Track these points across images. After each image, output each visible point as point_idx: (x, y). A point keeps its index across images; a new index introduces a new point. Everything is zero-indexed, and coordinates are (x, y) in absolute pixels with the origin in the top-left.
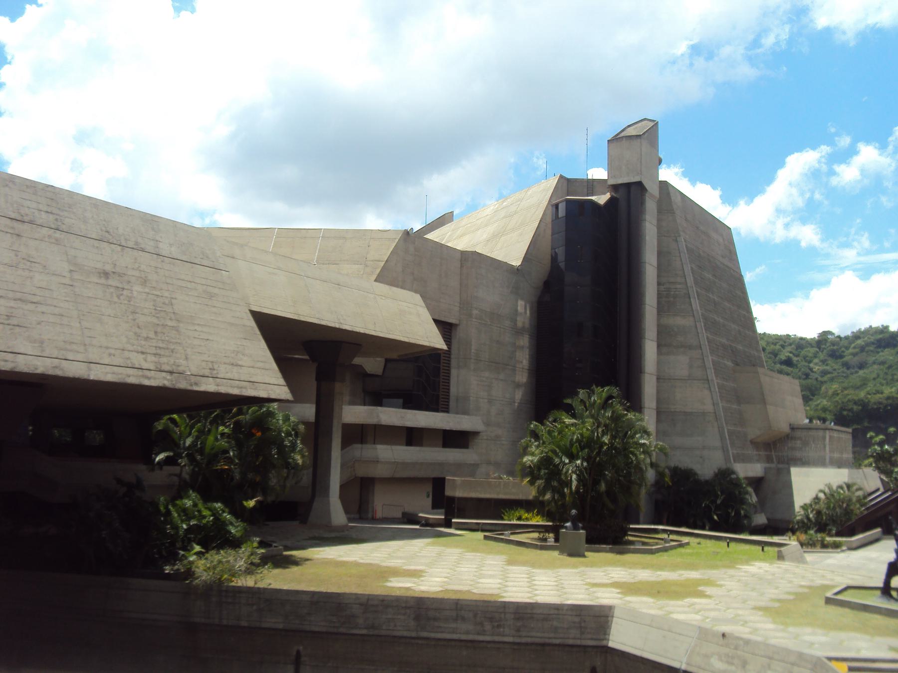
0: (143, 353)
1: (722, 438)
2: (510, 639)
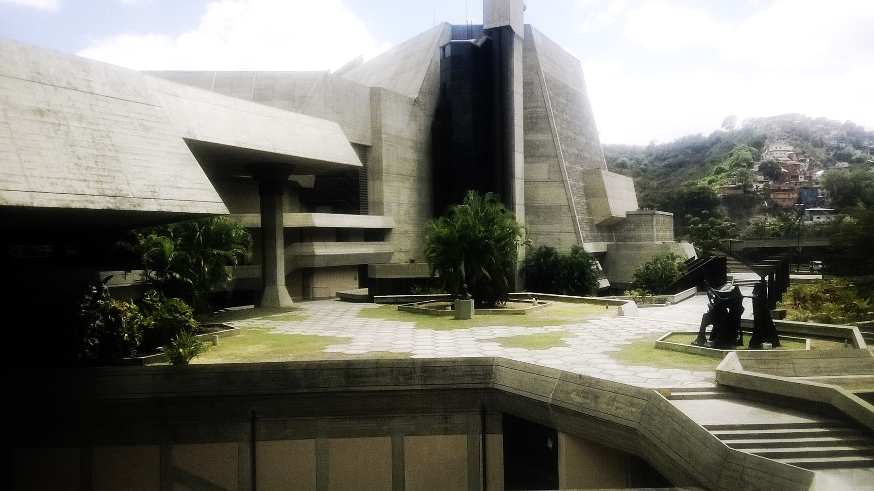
0: (85, 181)
2: (419, 388)
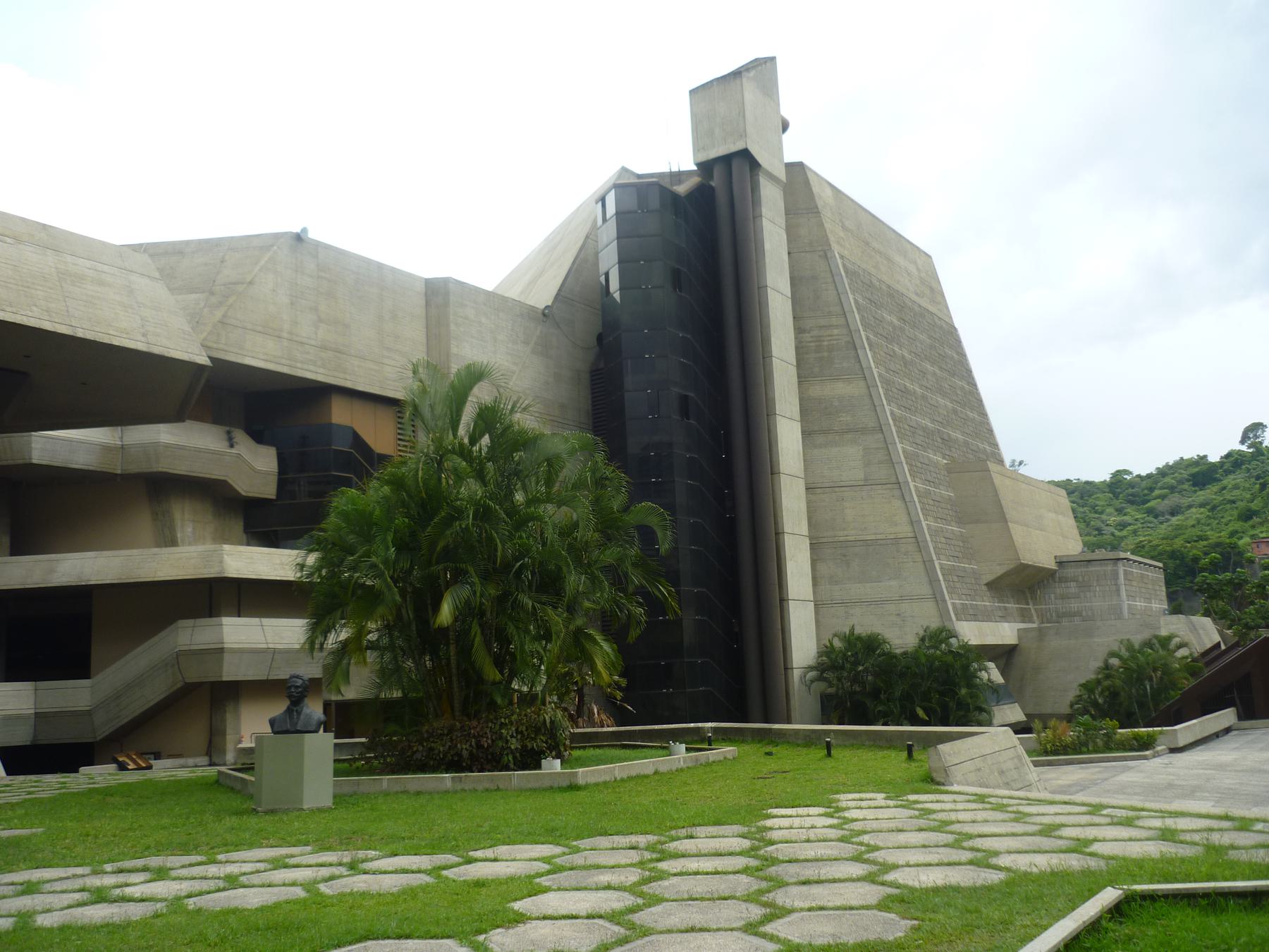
1: (933, 581)
